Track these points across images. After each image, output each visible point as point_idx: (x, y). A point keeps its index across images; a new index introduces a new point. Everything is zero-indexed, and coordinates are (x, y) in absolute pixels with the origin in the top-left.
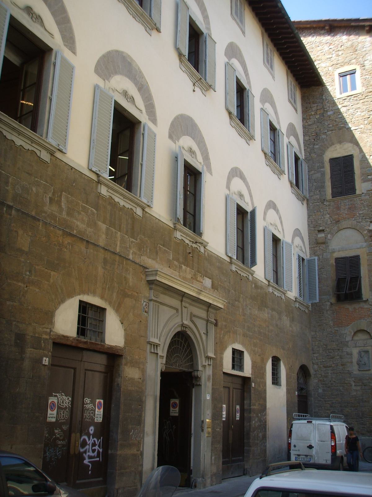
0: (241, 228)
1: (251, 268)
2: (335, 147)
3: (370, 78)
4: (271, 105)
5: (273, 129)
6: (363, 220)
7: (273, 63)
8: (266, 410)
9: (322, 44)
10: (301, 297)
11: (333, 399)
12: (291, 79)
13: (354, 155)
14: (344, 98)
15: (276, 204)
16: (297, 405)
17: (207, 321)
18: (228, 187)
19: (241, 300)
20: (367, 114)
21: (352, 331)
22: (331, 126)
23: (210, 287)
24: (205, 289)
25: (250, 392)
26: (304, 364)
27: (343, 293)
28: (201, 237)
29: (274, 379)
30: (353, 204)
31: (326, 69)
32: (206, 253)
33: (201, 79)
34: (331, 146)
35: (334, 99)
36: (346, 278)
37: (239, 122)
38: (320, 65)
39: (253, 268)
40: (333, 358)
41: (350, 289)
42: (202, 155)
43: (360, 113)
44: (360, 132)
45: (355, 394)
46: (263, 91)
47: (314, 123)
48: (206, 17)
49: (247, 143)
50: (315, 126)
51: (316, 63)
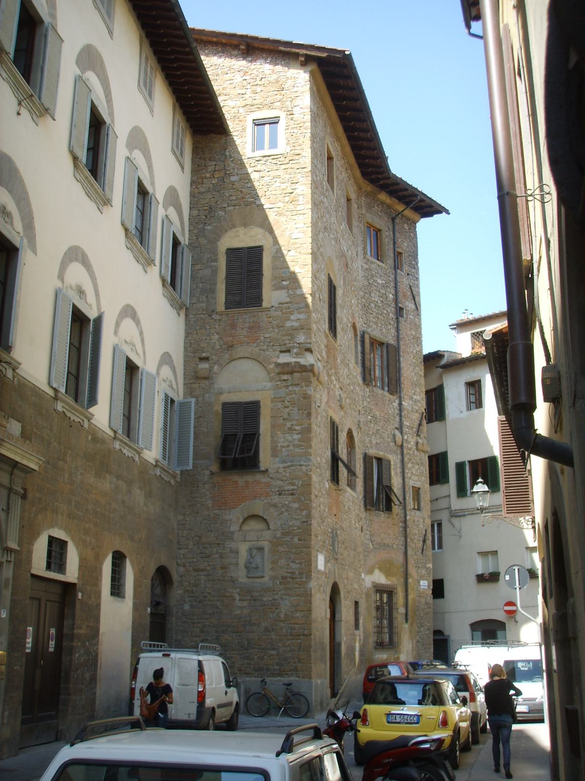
0: (76, 344)
1: (88, 408)
2: (238, 231)
3: (298, 133)
4: (143, 154)
5: (143, 192)
6: (269, 347)
7: (153, 87)
8: (99, 636)
9: (233, 71)
10: (165, 460)
11: (204, 621)
12: (179, 117)
13: (264, 247)
14: (257, 159)
15: (137, 310)
16: (148, 628)
17: (10, 490)
18: (61, 277)
19: (68, 459)
20: (289, 188)
21: (241, 517)
22: (234, 198)
23: (18, 435)
24: (9, 438)
25: (74, 606)
26: (163, 564)
27: (230, 457)
28: (10, 353)
29: (115, 587)
30: (257, 322)
31: (236, 110)
32: (16, 379)
33: (32, 96)
34: (231, 229)
35: (243, 158)
36: (236, 435)
37: (88, 174)
38: (226, 103)
39: (92, 410)
40: (209, 556)
41: (242, 452)
42: (23, 219)
43: (280, 185)
44: (276, 213)
45: (239, 612)
46: (132, 130)
47: (208, 191)
48: (109, 100)
49: (99, 209)
50: (209, 196)
51: (220, 99)
